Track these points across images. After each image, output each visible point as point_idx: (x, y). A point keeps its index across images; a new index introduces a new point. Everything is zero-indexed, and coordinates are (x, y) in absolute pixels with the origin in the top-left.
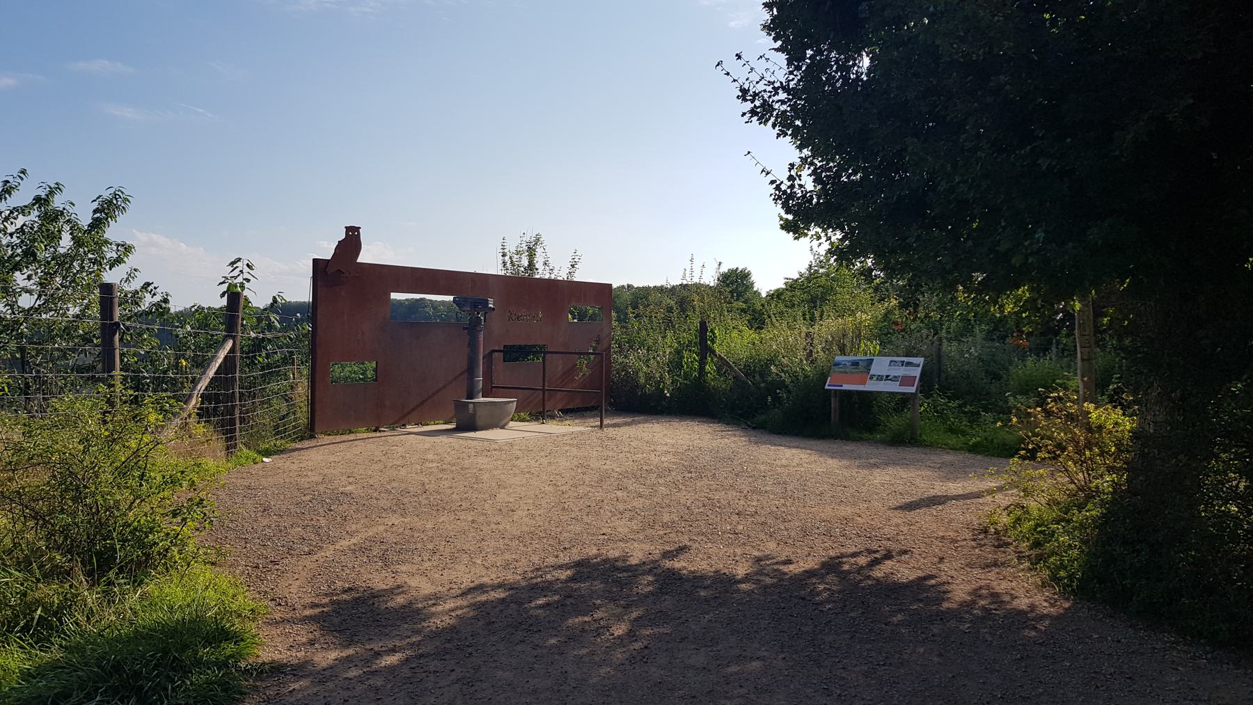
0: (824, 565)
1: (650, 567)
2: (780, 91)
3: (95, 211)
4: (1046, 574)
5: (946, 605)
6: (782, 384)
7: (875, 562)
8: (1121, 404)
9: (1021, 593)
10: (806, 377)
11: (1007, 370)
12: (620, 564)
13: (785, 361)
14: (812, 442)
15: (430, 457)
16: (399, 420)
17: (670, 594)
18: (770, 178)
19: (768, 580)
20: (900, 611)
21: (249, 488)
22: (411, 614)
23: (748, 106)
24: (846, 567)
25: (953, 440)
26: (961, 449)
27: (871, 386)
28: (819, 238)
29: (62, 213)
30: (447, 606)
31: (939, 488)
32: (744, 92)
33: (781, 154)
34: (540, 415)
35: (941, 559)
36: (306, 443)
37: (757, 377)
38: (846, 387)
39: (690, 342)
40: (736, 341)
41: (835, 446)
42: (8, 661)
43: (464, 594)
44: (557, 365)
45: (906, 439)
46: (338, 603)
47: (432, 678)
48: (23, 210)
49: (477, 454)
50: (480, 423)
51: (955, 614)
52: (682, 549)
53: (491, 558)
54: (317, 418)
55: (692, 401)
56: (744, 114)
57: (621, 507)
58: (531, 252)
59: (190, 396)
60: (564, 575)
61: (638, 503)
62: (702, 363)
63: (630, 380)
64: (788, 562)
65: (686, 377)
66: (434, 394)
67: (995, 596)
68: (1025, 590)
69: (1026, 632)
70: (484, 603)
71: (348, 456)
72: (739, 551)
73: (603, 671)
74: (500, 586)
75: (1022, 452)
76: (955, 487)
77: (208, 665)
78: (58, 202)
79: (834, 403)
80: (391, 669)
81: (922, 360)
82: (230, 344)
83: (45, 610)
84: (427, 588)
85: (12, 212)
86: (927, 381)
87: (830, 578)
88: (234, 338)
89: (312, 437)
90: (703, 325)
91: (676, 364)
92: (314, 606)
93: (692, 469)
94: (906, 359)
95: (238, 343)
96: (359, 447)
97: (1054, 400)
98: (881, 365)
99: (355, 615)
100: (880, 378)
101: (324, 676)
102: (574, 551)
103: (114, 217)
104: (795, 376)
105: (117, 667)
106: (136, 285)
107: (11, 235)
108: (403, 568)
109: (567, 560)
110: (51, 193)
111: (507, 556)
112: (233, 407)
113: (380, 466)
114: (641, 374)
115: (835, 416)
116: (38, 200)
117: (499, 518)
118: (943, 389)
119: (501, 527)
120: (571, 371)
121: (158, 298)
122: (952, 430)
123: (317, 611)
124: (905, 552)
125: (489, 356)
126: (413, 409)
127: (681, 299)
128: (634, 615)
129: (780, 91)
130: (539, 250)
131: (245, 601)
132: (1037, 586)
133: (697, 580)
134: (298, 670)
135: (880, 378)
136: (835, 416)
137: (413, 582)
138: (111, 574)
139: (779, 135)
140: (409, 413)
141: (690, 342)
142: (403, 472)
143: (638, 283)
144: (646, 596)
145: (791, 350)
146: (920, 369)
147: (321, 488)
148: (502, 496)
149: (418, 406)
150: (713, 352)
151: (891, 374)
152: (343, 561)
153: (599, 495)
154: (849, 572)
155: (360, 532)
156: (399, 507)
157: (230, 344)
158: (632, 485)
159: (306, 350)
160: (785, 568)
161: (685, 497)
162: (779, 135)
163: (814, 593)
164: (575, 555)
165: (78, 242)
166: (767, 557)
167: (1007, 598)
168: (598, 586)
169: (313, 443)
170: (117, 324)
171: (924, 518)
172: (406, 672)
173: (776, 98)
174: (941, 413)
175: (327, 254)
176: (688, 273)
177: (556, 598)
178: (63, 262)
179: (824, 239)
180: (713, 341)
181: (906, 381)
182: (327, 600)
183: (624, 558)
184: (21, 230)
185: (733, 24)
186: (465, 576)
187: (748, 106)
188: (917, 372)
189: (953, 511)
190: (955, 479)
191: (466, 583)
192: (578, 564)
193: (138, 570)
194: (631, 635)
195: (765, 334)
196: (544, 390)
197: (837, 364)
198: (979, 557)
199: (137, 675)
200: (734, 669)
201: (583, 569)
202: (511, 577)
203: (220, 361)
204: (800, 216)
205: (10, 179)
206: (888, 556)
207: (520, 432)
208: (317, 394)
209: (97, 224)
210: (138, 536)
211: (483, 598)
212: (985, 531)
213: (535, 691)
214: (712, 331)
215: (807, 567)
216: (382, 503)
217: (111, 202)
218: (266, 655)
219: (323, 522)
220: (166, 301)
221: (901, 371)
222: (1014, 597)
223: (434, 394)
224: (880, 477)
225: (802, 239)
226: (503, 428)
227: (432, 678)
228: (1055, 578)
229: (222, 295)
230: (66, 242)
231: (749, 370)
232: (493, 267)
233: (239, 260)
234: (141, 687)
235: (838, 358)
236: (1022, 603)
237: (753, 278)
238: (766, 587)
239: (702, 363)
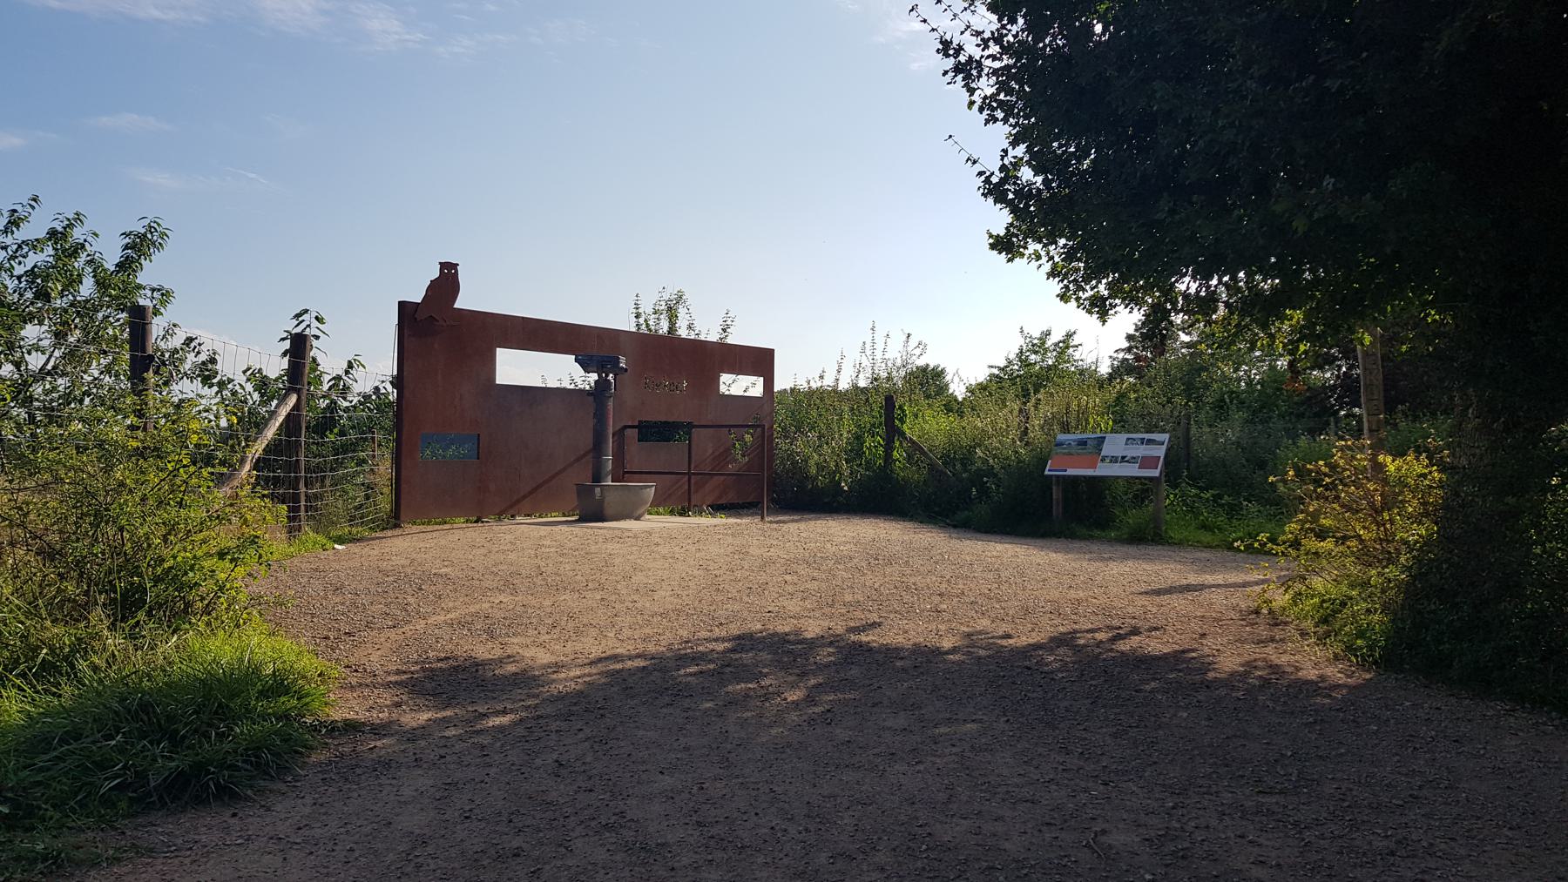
0: (1052, 639)
1: (833, 640)
2: (991, 43)
3: (126, 247)
4: (1338, 648)
5: (1211, 675)
6: (990, 472)
7: (1119, 637)
8: (1427, 450)
9: (1309, 665)
10: (1019, 462)
11: (1274, 453)
12: (791, 637)
15: (547, 543)
16: (509, 508)
18: (978, 168)
19: (982, 653)
20: (1154, 679)
21: (316, 570)
22: (525, 680)
23: (950, 63)
24: (1082, 642)
25: (1206, 537)
26: (1218, 546)
27: (1103, 470)
28: (1039, 257)
29: (83, 246)
30: (572, 674)
31: (1193, 579)
33: (993, 143)
35: (1203, 635)
36: (389, 533)
37: (958, 466)
38: (1071, 472)
39: (873, 425)
40: (927, 426)
42: (7, 707)
43: (591, 663)
44: (705, 444)
45: (1147, 537)
46: (432, 670)
47: (553, 736)
48: (35, 245)
49: (606, 540)
50: (608, 511)
52: (874, 625)
53: (626, 632)
54: (403, 502)
55: (877, 495)
56: (945, 73)
57: (790, 589)
58: (672, 313)
59: (242, 461)
60: (720, 647)
61: (814, 585)
62: (889, 448)
63: (797, 471)
64: (1009, 636)
66: (553, 477)
67: (1275, 668)
68: (1312, 661)
69: (1319, 700)
70: (618, 672)
71: (443, 542)
72: (943, 627)
73: (774, 732)
74: (638, 656)
75: (1301, 516)
77: (264, 717)
78: (78, 234)
79: (1056, 493)
80: (501, 729)
81: (1166, 436)
82: (293, 399)
83: (52, 649)
84: (544, 658)
85: (20, 246)
86: (1178, 464)
87: (1061, 651)
88: (298, 392)
89: (397, 526)
91: (855, 451)
92: (398, 672)
93: (877, 558)
94: (1147, 436)
95: (303, 398)
96: (457, 534)
97: (1341, 449)
99: (451, 681)
100: (1114, 460)
101: (413, 735)
102: (732, 626)
103: (148, 256)
105: (145, 707)
106: (177, 341)
107: (19, 278)
108: (515, 640)
109: (724, 634)
110: (70, 226)
111: (648, 631)
112: (297, 479)
113: (483, 551)
114: (812, 462)
115: (1057, 510)
116: (53, 234)
117: (636, 598)
118: (1194, 480)
119: (638, 605)
120: (725, 455)
121: (203, 357)
122: (1204, 527)
123: (404, 677)
124: (1156, 629)
125: (620, 434)
126: (524, 497)
128: (812, 682)
129: (991, 43)
130: (682, 312)
131: (309, 664)
132: (1328, 660)
133: (892, 653)
134: (378, 730)
135: (1114, 460)
136: (1057, 510)
137: (528, 653)
138: (141, 615)
139: (987, 122)
140: (518, 501)
141: (873, 425)
142: (512, 556)
144: (827, 666)
146: (1164, 447)
147: (409, 571)
148: (638, 578)
149: (530, 493)
150: (903, 434)
152: (442, 632)
153: (763, 578)
154: (1085, 646)
155: (457, 608)
156: (509, 586)
157: (293, 399)
158: (803, 570)
159: (388, 423)
160: (1004, 642)
161: (869, 579)
162: (987, 122)
163: (1041, 663)
164: (735, 629)
165: (102, 284)
166: (980, 633)
167: (1289, 670)
168: (766, 656)
169: (398, 532)
170: (151, 358)
171: (1178, 602)
172: (520, 731)
173: (986, 53)
174: (1192, 510)
175: (417, 296)
176: (868, 346)
177: (712, 666)
178: (85, 309)
179: (1044, 259)
180: (902, 421)
181: (1147, 462)
182: (417, 668)
183: (798, 632)
184: (31, 273)
185: (915, 66)
186: (594, 647)
187: (950, 63)
188: (1160, 452)
190: (1213, 572)
191: (596, 652)
192: (739, 637)
193: (177, 613)
194: (810, 700)
196: (689, 474)
197: (1059, 444)
198: (1251, 633)
199: (171, 718)
200: (942, 730)
201: (744, 642)
202: (652, 648)
203: (281, 419)
205: (19, 208)
206: (1135, 632)
208: (404, 473)
209: (126, 265)
210: (173, 578)
211: (619, 666)
212: (1257, 612)
213: (686, 749)
214: (901, 408)
215: (1031, 641)
216: (486, 584)
217: (145, 235)
218: (337, 715)
219: (411, 600)
220: (213, 361)
222: (1298, 669)
223: (553, 477)
225: (1017, 260)
226: (638, 518)
227: (553, 736)
228: (1350, 649)
229: (285, 354)
230: (87, 288)
231: (947, 459)
233: (306, 311)
234: (177, 731)
235: (1061, 437)
236: (1311, 674)
238: (980, 658)
239: (889, 448)
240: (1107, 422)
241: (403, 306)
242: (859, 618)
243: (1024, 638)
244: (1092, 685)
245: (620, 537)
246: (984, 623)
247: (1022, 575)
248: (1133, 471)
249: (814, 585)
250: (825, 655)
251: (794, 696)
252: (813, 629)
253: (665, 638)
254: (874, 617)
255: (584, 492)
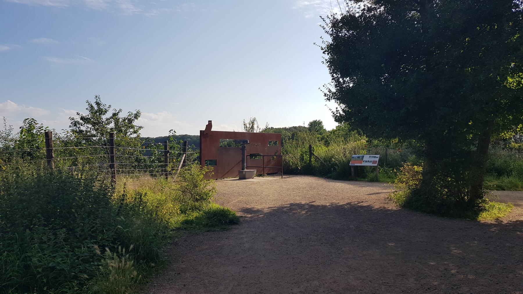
6: (336, 164)
13: (337, 157)
14: (346, 182)
17: (313, 209)
23: (326, 97)
25: (389, 180)
27: (363, 164)
32: (325, 94)
34: (260, 175)
38: (356, 165)
40: (321, 151)
41: (352, 182)
45: (375, 180)
50: (247, 177)
51: (374, 210)
52: (314, 202)
55: (308, 170)
61: (300, 194)
62: (310, 158)
65: (305, 163)
76: (384, 191)
86: (381, 162)
90: (310, 146)
91: (302, 159)
98: (367, 158)
100: (366, 161)
104: (340, 162)
115: (353, 174)
118: (387, 165)
122: (389, 178)
127: (295, 133)
130: (255, 122)
133: (318, 206)
135: (366, 161)
143: (276, 126)
145: (339, 154)
150: (314, 154)
151: (369, 160)
174: (387, 173)
175: (204, 129)
181: (374, 162)
185: (307, 17)
187: (326, 97)
188: (377, 160)
189: (382, 195)
194: (306, 213)
195: (330, 148)
201: (291, 205)
204: (338, 119)
206: (362, 202)
207: (257, 179)
221: (373, 159)
224: (365, 189)
231: (325, 160)
232: (240, 129)
235: (353, 156)
237: (323, 124)
239: (310, 158)
240: (365, 152)
241: (201, 131)
242: (311, 200)
243: (341, 203)
244: (354, 212)
245: (253, 183)
246: (335, 201)
247: (343, 191)
248: (371, 164)
249: (300, 194)
250: (307, 207)
251: (304, 212)
252: (303, 202)
253: (278, 204)
254: (314, 200)
255: (240, 173)
